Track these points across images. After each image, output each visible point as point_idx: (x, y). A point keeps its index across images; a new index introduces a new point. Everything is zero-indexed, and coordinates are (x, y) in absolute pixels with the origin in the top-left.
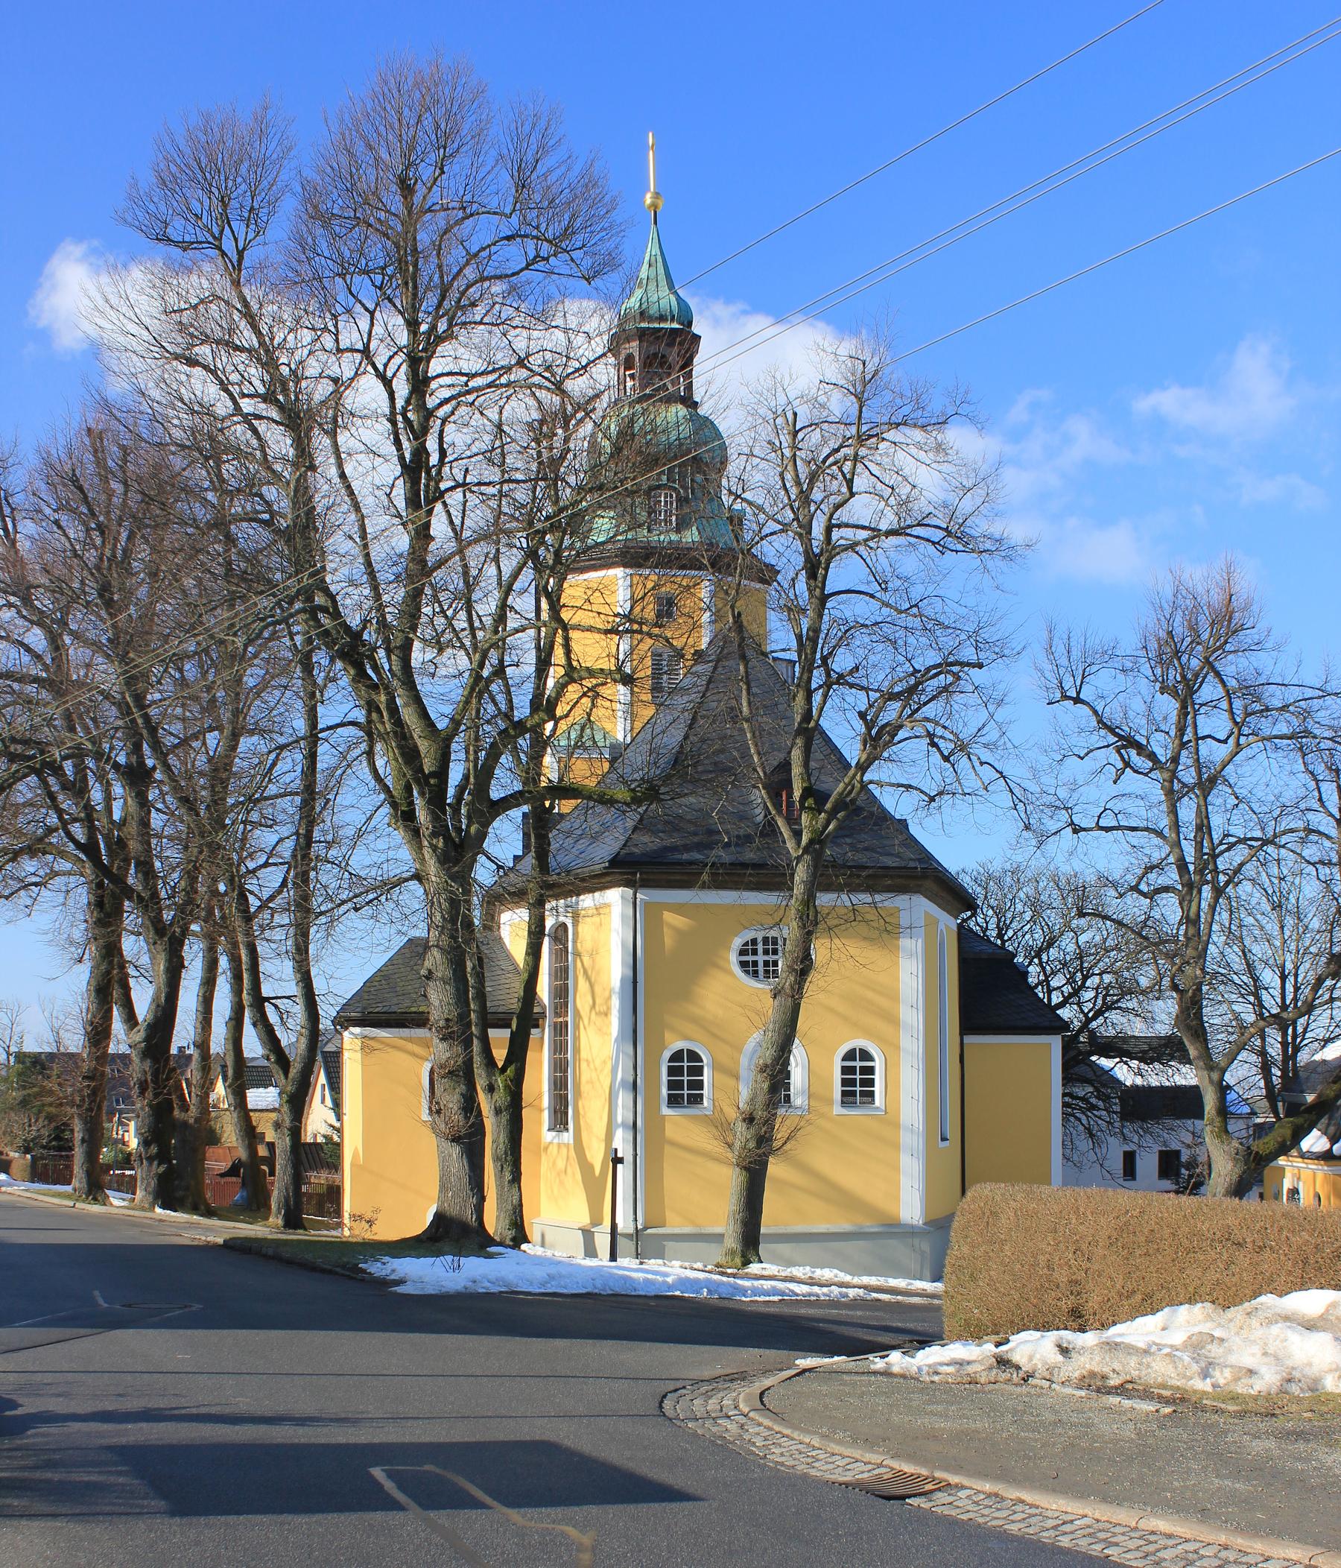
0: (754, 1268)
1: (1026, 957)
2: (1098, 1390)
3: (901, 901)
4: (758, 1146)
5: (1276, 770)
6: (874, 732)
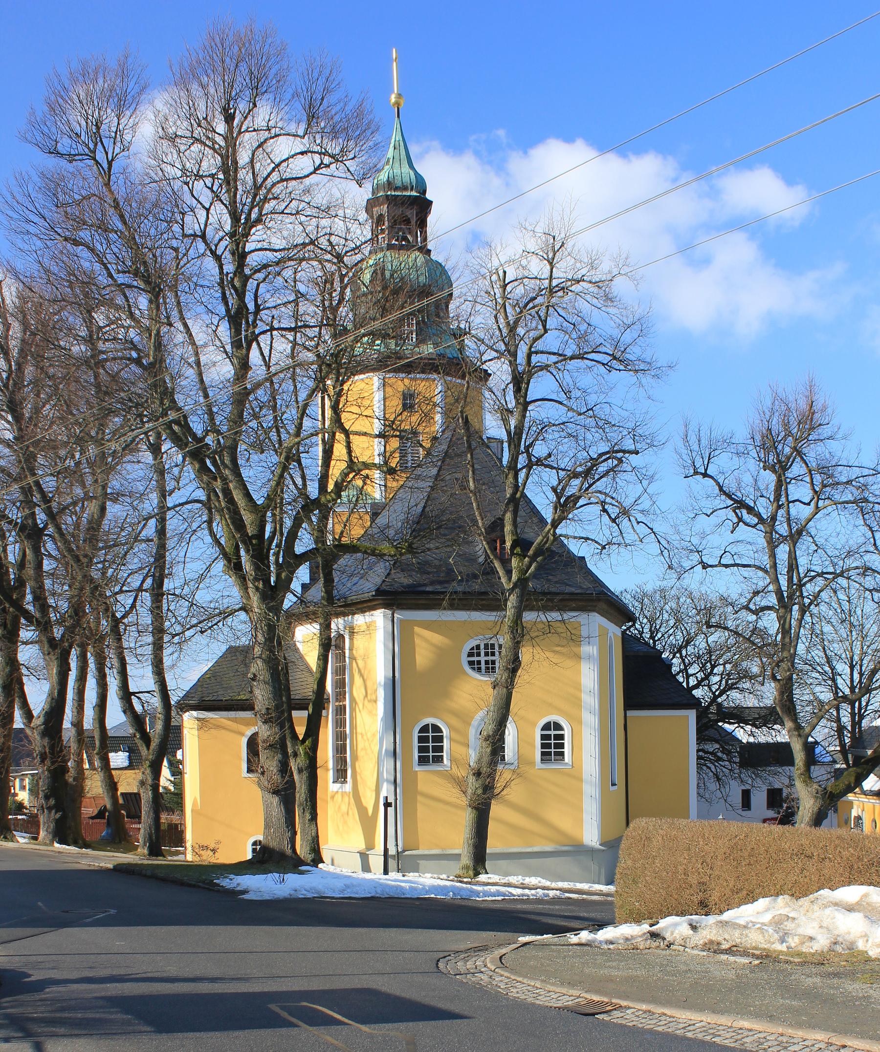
0: (483, 878)
1: (670, 652)
2: (715, 952)
3: (583, 618)
4: (484, 793)
5: (844, 523)
6: (562, 500)
